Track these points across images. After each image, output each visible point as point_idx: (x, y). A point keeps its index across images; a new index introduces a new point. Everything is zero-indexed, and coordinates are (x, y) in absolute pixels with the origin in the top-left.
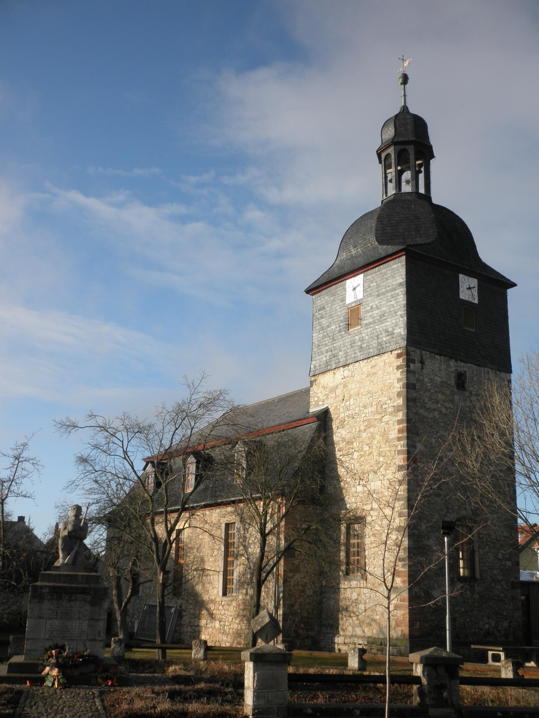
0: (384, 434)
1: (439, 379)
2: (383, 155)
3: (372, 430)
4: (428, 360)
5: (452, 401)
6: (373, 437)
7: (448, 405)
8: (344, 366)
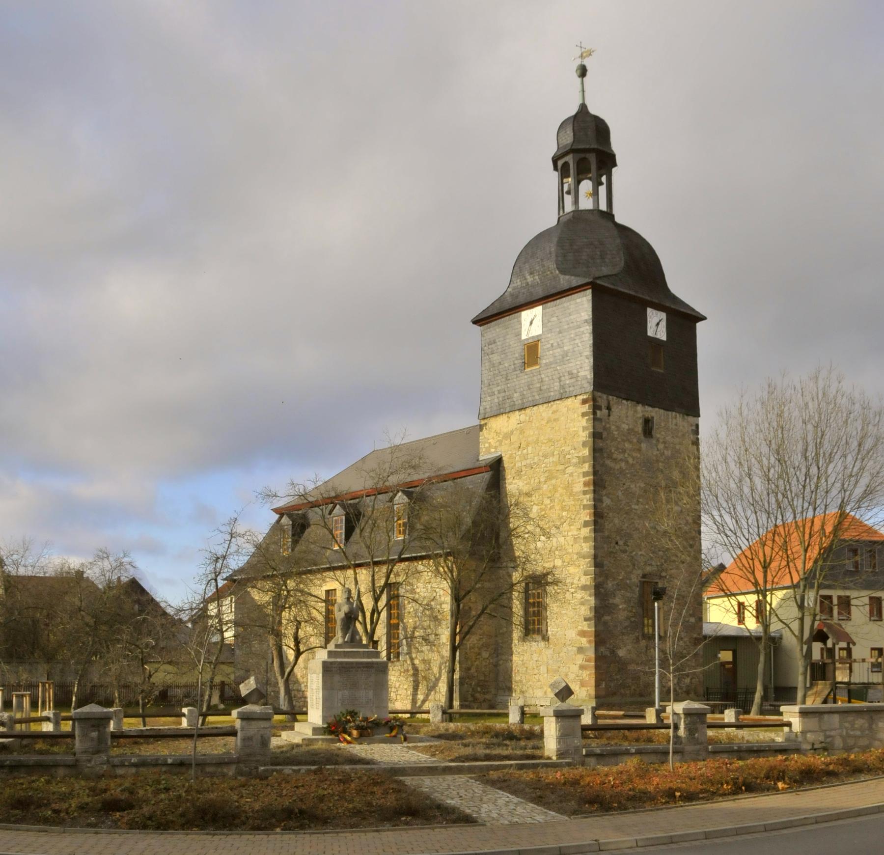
0: (568, 487)
1: (626, 427)
2: (560, 163)
3: (554, 481)
4: (615, 406)
5: (639, 450)
6: (555, 489)
7: (634, 454)
8: (520, 410)
